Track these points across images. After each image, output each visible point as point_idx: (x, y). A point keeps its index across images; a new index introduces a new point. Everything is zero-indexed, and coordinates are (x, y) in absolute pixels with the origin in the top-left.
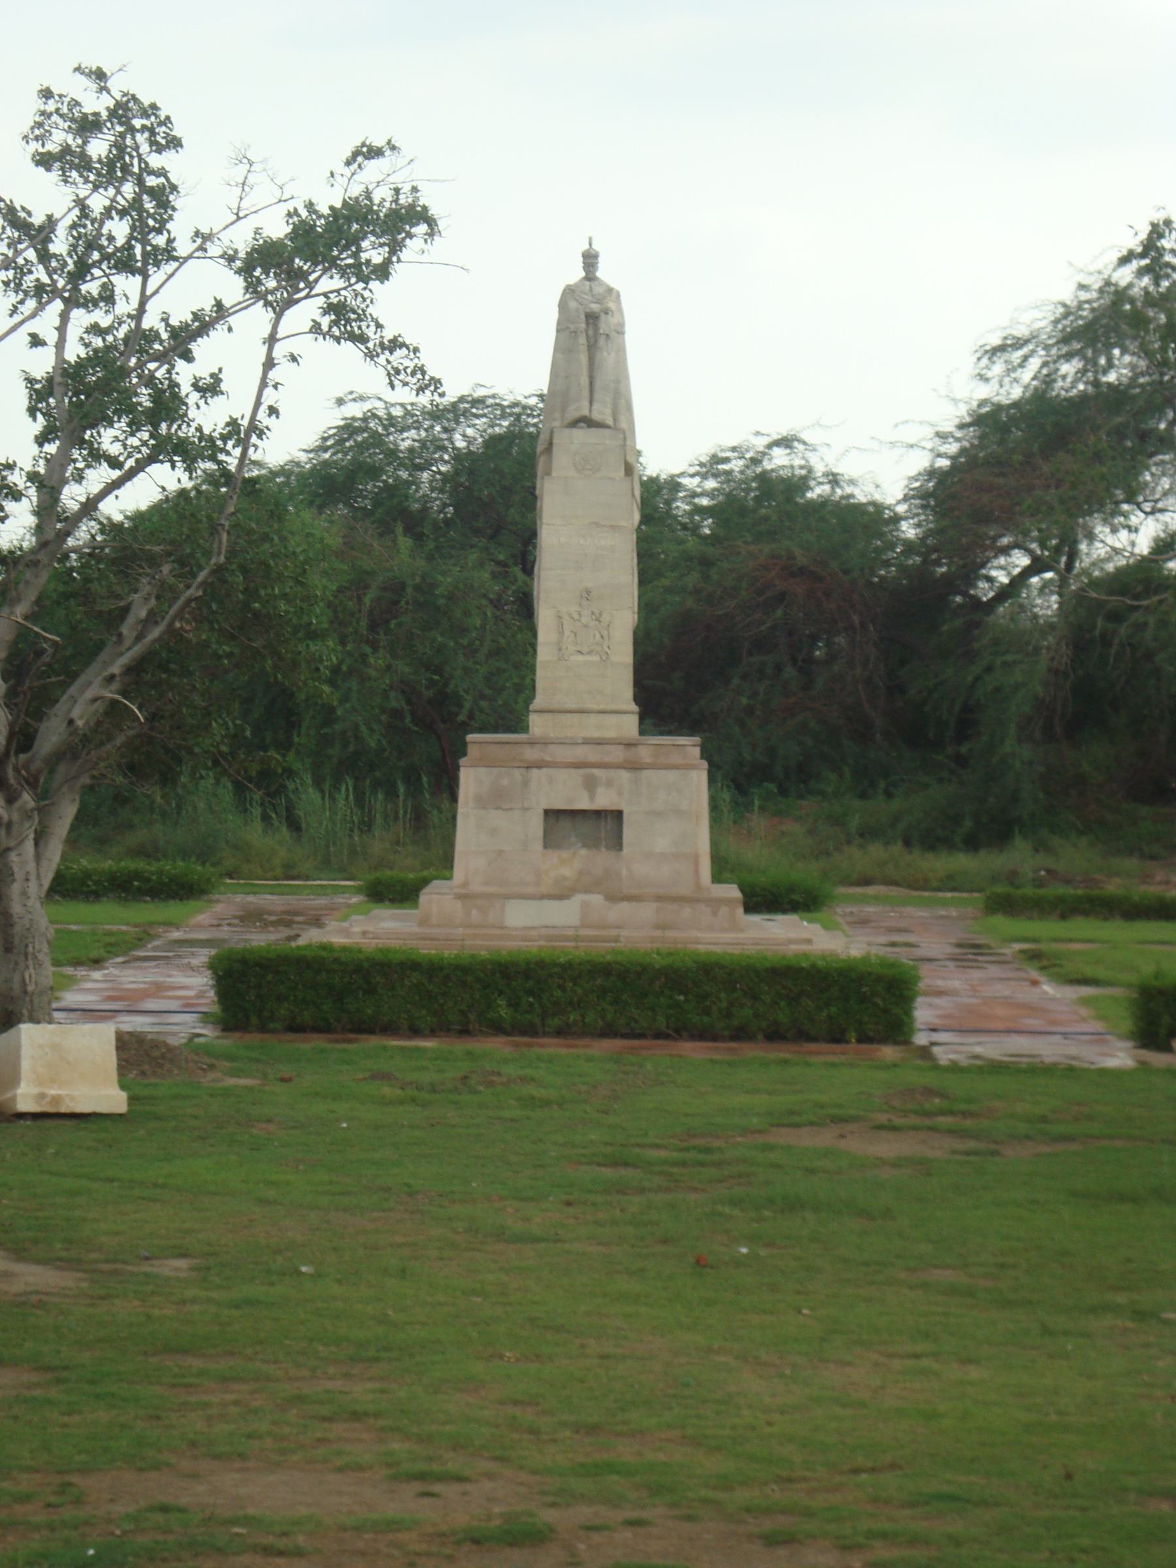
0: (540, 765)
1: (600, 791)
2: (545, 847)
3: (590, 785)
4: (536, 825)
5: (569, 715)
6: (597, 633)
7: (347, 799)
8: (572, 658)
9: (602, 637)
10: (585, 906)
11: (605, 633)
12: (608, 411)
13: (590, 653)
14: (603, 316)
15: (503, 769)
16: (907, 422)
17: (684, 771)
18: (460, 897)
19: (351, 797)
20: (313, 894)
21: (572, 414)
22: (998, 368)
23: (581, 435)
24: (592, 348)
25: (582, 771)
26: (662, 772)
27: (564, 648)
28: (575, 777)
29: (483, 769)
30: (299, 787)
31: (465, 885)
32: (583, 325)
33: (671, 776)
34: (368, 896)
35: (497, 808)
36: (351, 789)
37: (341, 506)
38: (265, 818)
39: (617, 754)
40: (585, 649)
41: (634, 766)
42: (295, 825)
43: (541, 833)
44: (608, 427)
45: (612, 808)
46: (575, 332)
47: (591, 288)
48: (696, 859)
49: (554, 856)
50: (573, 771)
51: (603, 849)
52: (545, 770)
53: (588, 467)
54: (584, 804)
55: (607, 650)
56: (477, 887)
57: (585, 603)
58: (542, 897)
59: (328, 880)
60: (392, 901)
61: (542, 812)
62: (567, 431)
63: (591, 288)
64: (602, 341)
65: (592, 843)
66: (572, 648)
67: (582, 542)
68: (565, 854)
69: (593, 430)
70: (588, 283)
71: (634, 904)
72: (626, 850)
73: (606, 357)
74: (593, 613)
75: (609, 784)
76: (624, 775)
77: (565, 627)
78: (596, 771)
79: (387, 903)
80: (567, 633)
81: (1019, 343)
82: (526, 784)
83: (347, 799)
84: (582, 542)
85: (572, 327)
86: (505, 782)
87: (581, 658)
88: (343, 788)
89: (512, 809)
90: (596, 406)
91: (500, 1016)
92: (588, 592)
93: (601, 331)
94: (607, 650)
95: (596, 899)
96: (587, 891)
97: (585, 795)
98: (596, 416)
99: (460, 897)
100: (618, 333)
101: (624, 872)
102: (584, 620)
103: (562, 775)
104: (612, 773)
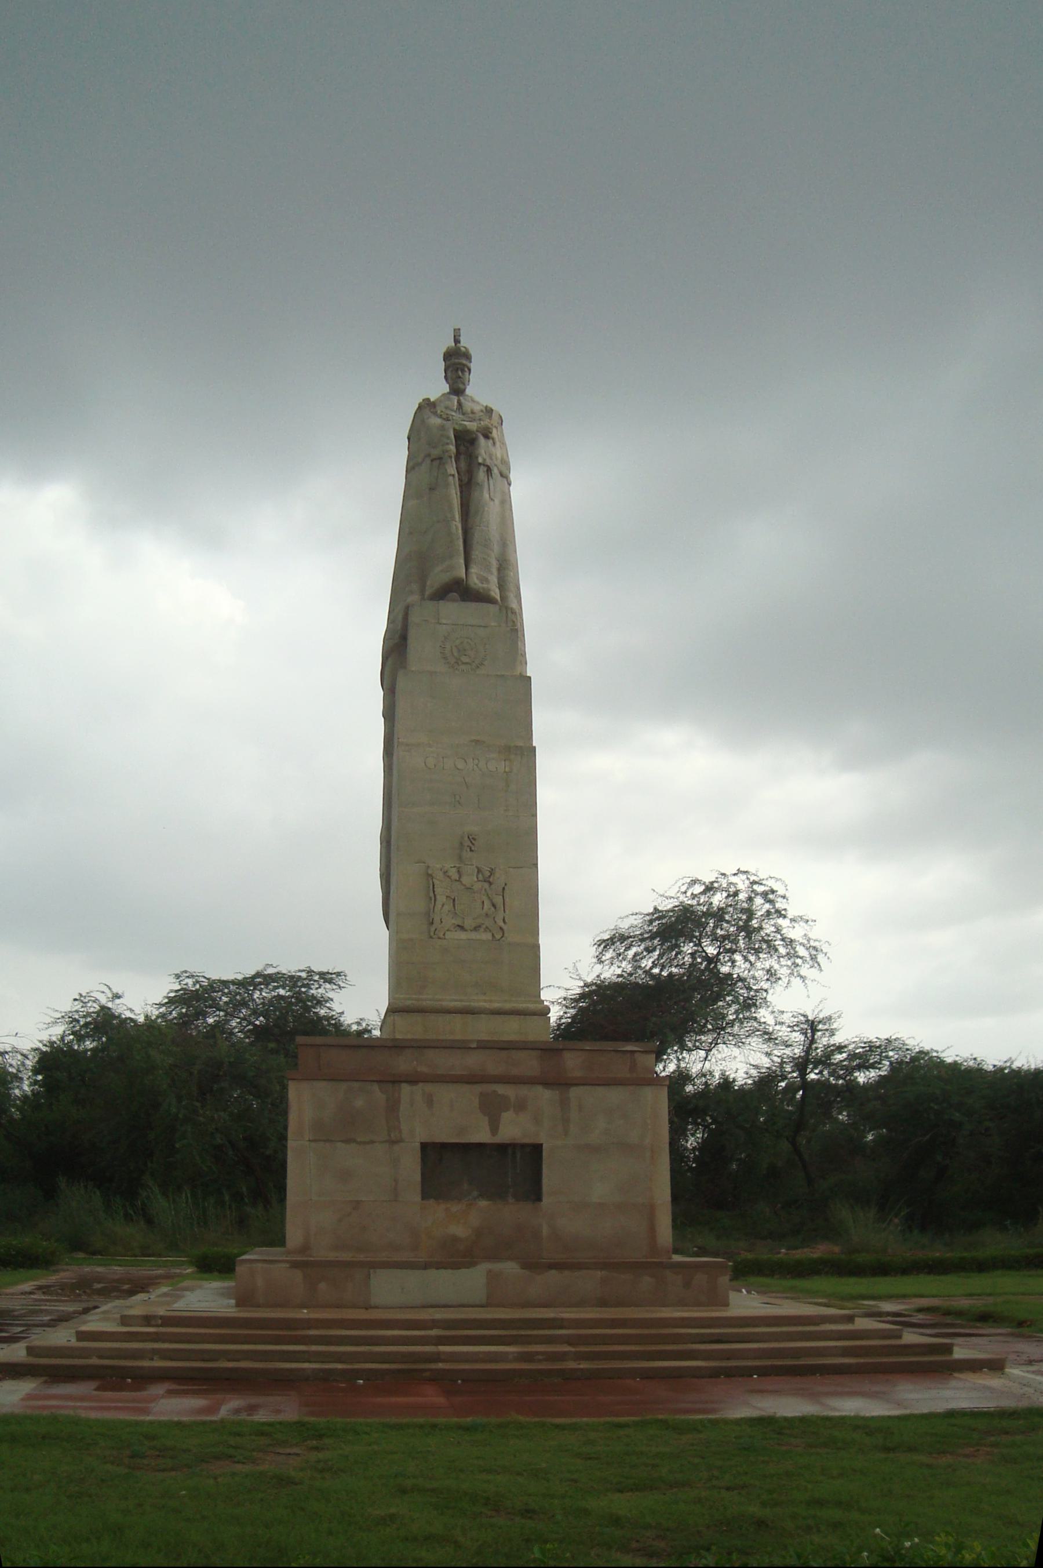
0: (413, 1080)
1: (507, 1116)
2: (425, 1196)
3: (492, 1109)
4: (411, 1167)
5: (448, 1017)
6: (485, 898)
7: (187, 1202)
8: (449, 935)
9: (494, 906)
10: (491, 1276)
11: (498, 900)
12: (494, 579)
13: (476, 929)
14: (482, 440)
15: (356, 1085)
16: (550, 986)
17: (632, 1088)
18: (295, 1265)
19: (190, 1200)
20: (155, 1266)
21: (438, 577)
22: (609, 954)
23: (453, 610)
24: (467, 485)
25: (478, 1088)
26: (601, 1090)
27: (437, 920)
28: (468, 1096)
29: (322, 1084)
30: (151, 1194)
31: (305, 1248)
32: (452, 448)
33: (615, 1096)
34: (198, 1267)
35: (348, 1141)
36: (189, 1195)
37: (176, 1015)
38: (126, 1215)
39: (529, 1064)
40: (468, 923)
41: (559, 1083)
42: (150, 1222)
43: (418, 1177)
44: (490, 600)
45: (526, 1141)
46: (440, 458)
47: (460, 404)
48: (651, 1211)
49: (438, 1211)
50: (466, 1088)
51: (511, 1200)
52: (421, 1085)
53: (465, 659)
54: (483, 1136)
55: (502, 924)
56: (322, 1253)
57: (467, 854)
58: (426, 1266)
59: (177, 1257)
60: (220, 1272)
61: (418, 1145)
62: (430, 605)
63: (460, 404)
64: (481, 474)
65: (496, 1193)
66: (450, 921)
67: (460, 765)
68: (455, 1208)
69: (473, 605)
70: (455, 399)
71: (567, 1273)
72: (546, 1200)
73: (486, 495)
74: (479, 871)
75: (521, 1106)
76: (544, 1096)
77: (438, 890)
78: (501, 1089)
79: (216, 1274)
80: (441, 899)
81: (623, 938)
82: (393, 1108)
83: (187, 1202)
84: (460, 765)
85: (435, 453)
86: (359, 1103)
87: (463, 936)
88: (184, 1195)
89: (372, 1142)
90: (474, 570)
91: (91, 1050)
92: (472, 839)
93: (480, 460)
94: (502, 924)
95: (510, 1268)
96: (493, 1256)
97: (484, 1122)
98: (475, 582)
99: (295, 1265)
100: (502, 475)
101: (545, 1231)
102: (465, 880)
103: (445, 1094)
104: (524, 1091)
